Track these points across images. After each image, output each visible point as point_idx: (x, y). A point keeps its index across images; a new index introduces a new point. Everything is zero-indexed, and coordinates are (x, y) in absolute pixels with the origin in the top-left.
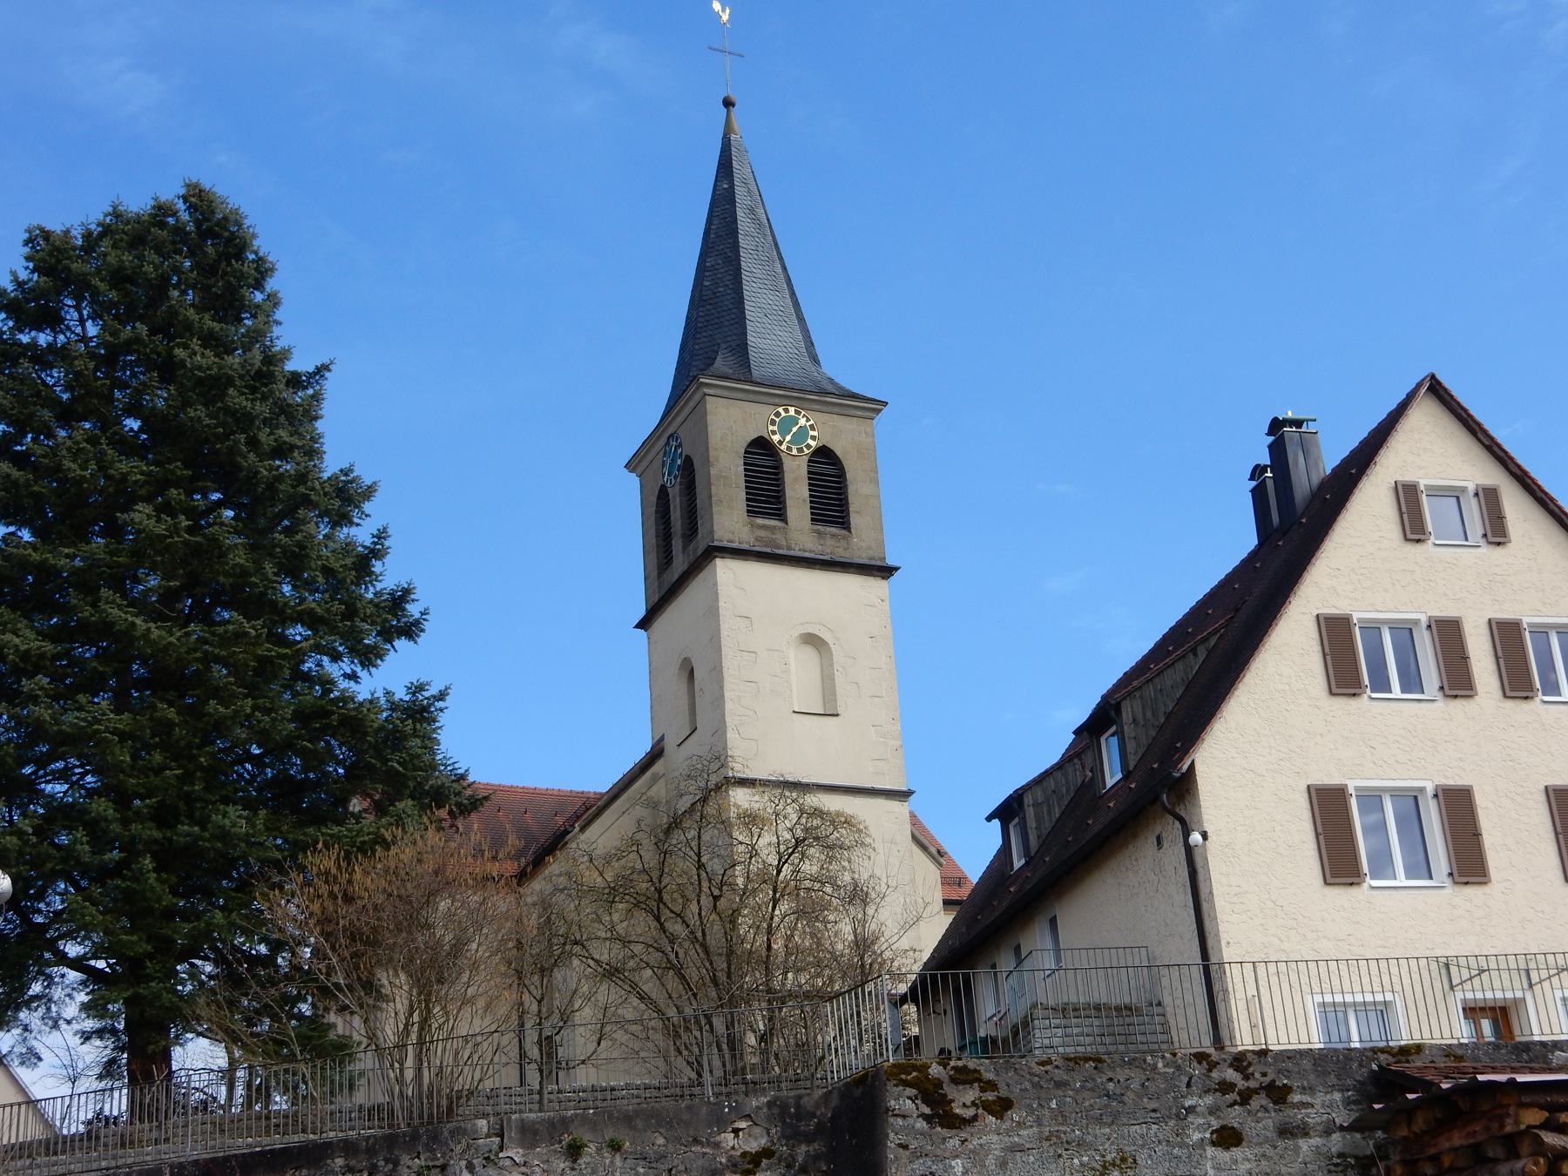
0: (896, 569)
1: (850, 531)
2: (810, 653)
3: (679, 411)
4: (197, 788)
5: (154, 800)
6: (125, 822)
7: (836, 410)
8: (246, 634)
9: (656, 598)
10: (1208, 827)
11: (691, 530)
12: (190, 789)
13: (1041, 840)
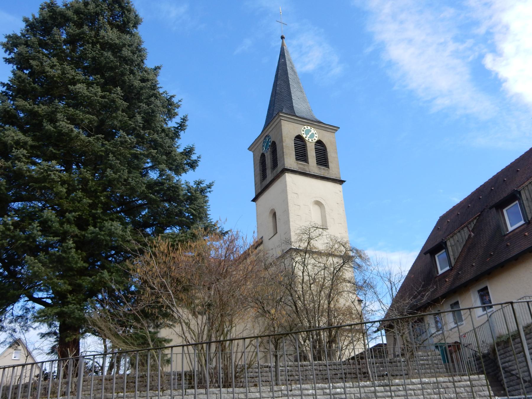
0: (344, 181)
1: (329, 168)
2: (317, 207)
3: (270, 127)
4: (98, 211)
5: (77, 213)
6: (61, 224)
7: (323, 129)
8: (126, 142)
9: (260, 191)
10: (166, 335)
11: (275, 164)
12: (95, 212)
13: (456, 260)
